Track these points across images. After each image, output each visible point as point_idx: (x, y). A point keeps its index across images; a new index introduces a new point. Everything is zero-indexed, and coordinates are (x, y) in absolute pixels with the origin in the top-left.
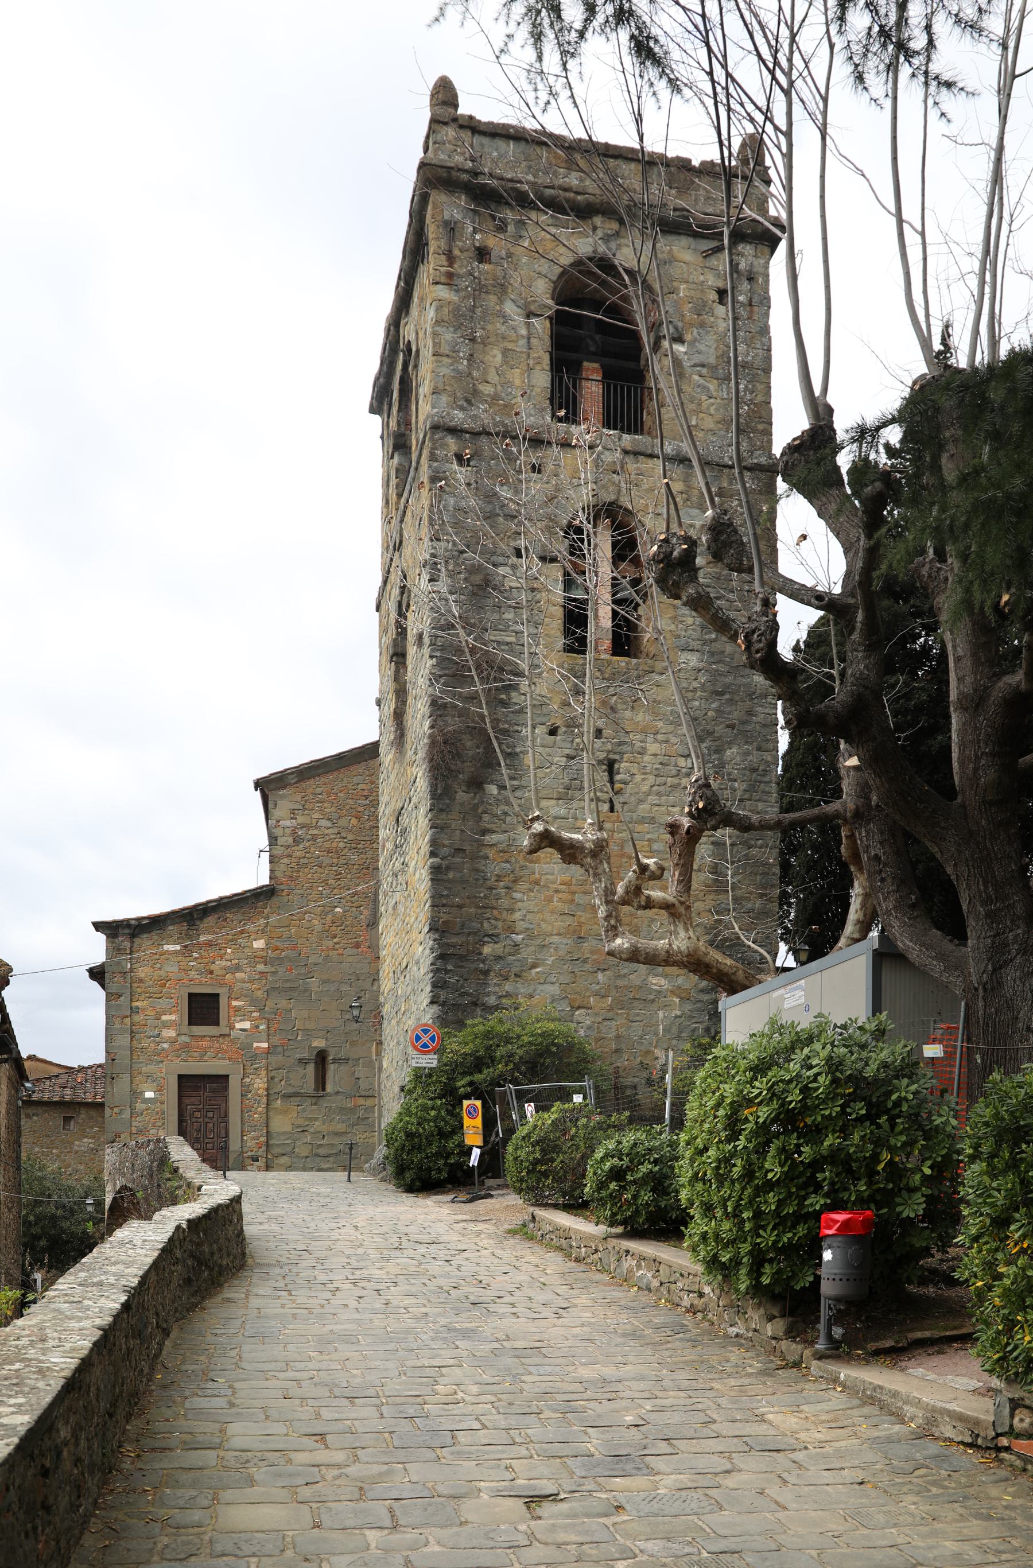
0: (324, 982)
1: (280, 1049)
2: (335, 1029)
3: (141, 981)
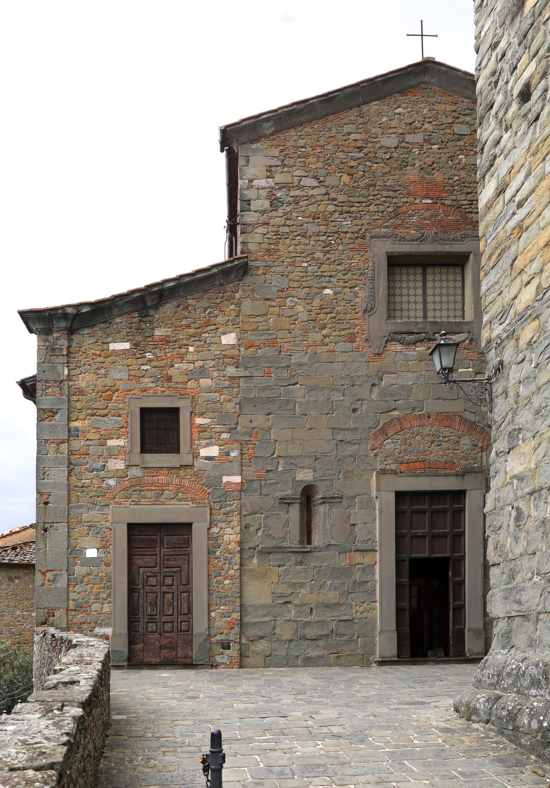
0: (312, 389)
1: (256, 485)
2: (325, 455)
3: (81, 392)
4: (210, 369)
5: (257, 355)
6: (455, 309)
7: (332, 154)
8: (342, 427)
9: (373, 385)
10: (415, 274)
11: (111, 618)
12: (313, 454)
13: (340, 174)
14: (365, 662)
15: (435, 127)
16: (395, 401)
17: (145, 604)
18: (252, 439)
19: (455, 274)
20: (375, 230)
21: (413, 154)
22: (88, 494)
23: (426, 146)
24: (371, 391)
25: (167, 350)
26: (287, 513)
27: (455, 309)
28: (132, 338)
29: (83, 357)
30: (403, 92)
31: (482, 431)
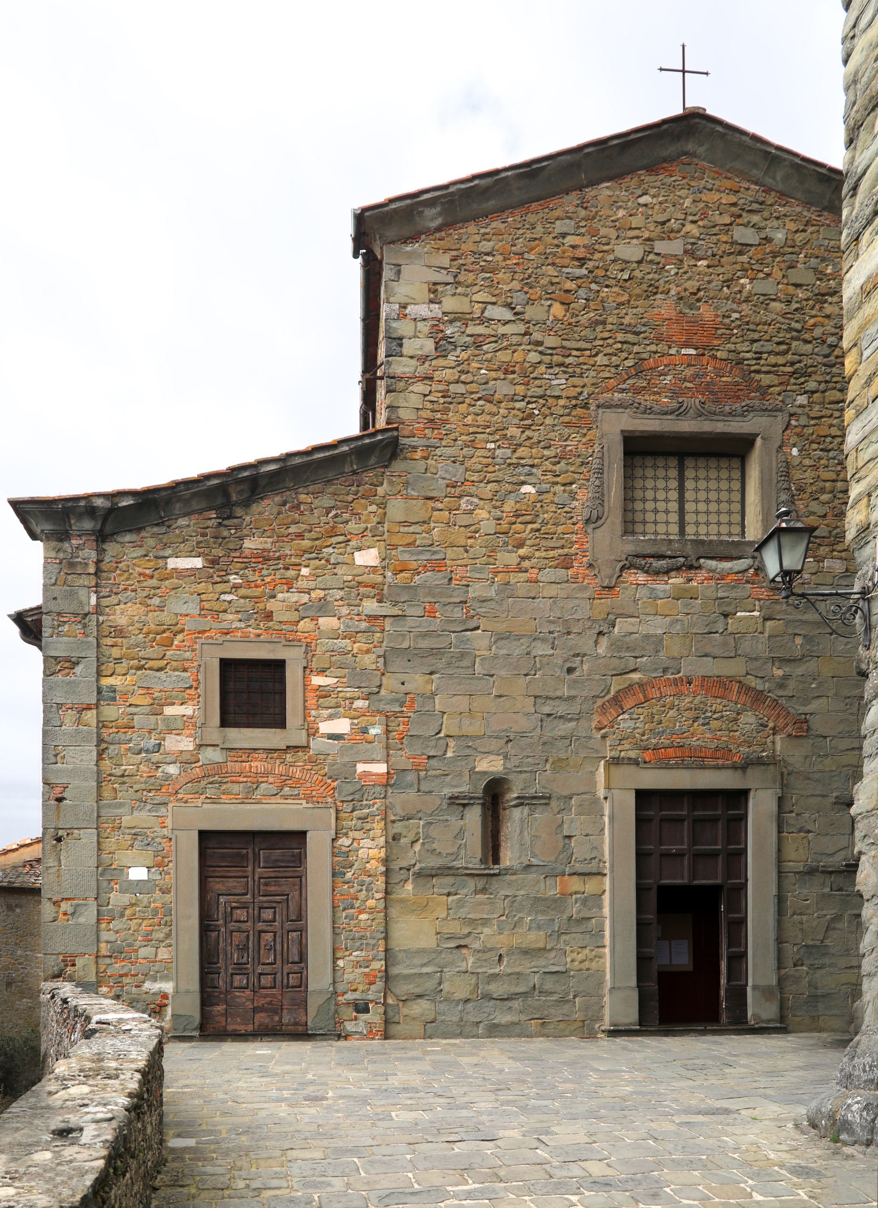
0: (501, 637)
1: (411, 777)
2: (522, 735)
3: (119, 632)
4: (336, 603)
5: (412, 584)
6: (730, 524)
7: (536, 268)
8: (550, 694)
9: (600, 633)
10: (666, 468)
11: (171, 968)
12: (503, 734)
13: (549, 302)
14: (586, 1031)
15: (702, 230)
16: (636, 657)
17: (229, 948)
18: (405, 709)
19: (730, 469)
20: (605, 395)
21: (667, 274)
22: (131, 787)
23: (688, 262)
24: (596, 643)
25: (264, 572)
26: (462, 819)
27: (730, 524)
28: (207, 551)
29: (122, 578)
30: (652, 168)
31: (774, 704)
